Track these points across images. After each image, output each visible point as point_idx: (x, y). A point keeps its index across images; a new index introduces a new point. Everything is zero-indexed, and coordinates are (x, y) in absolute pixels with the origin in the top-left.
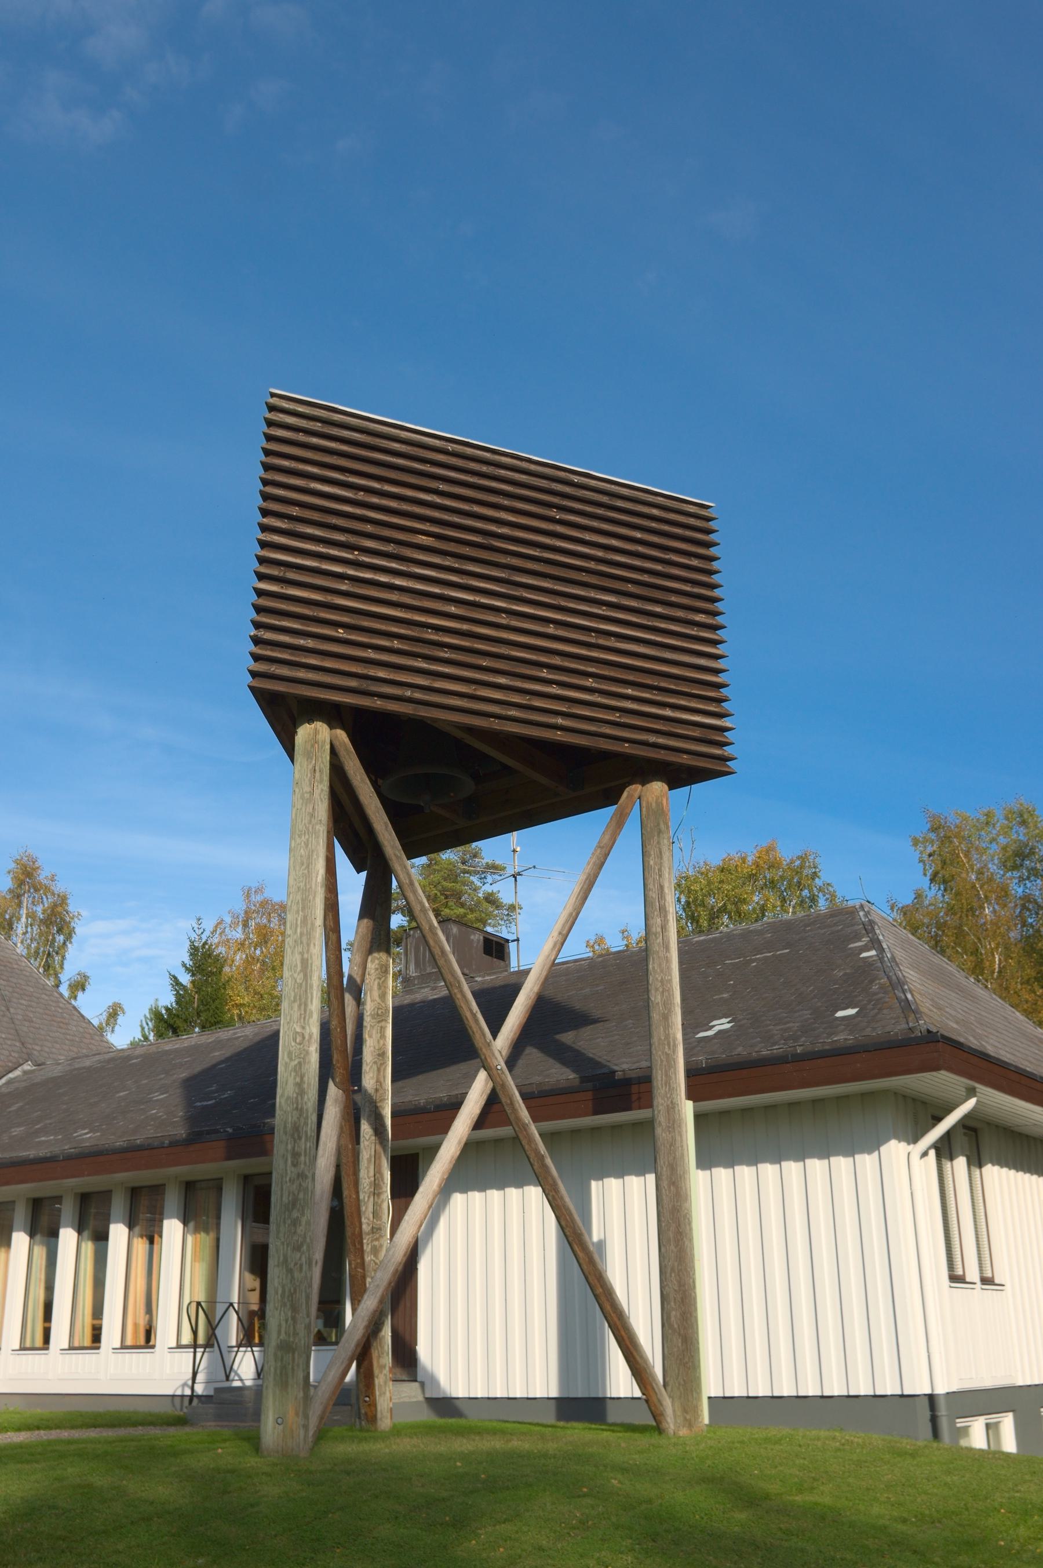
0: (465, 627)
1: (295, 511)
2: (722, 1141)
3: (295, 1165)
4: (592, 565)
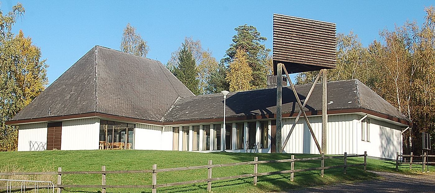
0: (300, 49)
1: (278, 33)
2: (330, 119)
3: (279, 122)
4: (317, 37)
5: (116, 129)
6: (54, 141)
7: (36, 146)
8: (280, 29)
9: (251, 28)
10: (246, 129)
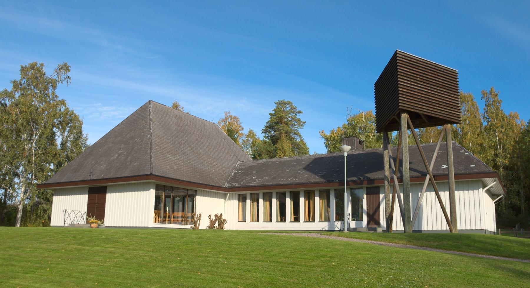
5: (175, 196)
6: (96, 210)
7: (72, 216)
8: (405, 69)
9: (288, 103)
10: (275, 201)
